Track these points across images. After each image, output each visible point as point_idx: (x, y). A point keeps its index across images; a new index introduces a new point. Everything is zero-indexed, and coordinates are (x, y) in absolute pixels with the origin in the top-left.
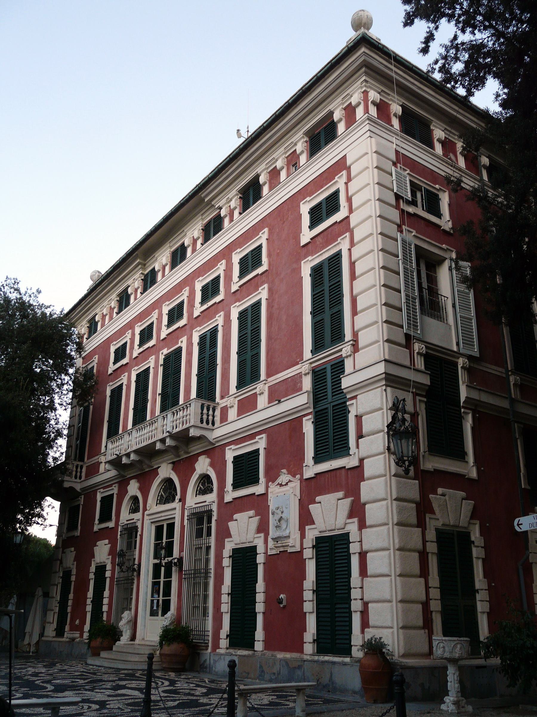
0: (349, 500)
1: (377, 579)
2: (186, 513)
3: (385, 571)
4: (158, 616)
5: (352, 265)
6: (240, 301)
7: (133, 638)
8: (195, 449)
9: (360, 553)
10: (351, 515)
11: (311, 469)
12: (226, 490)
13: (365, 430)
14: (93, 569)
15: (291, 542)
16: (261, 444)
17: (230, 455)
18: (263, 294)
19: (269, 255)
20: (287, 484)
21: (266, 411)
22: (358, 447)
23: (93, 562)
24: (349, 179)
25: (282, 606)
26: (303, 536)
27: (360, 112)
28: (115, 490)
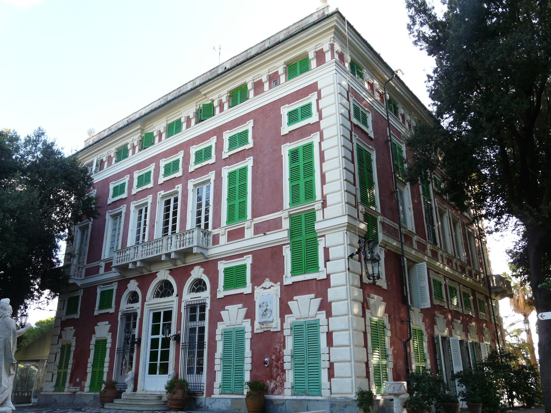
0: (319, 299)
1: (339, 348)
2: (183, 305)
3: (347, 343)
4: (156, 374)
5: (322, 154)
6: (229, 165)
7: (135, 389)
8: (190, 261)
9: (327, 333)
10: (320, 309)
11: (289, 280)
12: (218, 290)
13: (331, 257)
14: (93, 342)
15: (274, 325)
16: (248, 261)
17: (222, 266)
18: (249, 163)
19: (254, 137)
20: (270, 288)
21: (252, 240)
22: (325, 266)
23: (93, 338)
24: (319, 97)
25: (266, 365)
26: (283, 321)
27: (328, 56)
28: (115, 287)
